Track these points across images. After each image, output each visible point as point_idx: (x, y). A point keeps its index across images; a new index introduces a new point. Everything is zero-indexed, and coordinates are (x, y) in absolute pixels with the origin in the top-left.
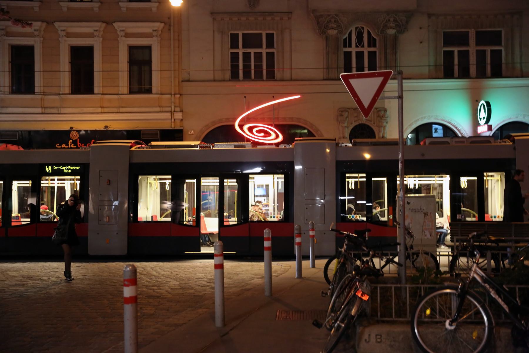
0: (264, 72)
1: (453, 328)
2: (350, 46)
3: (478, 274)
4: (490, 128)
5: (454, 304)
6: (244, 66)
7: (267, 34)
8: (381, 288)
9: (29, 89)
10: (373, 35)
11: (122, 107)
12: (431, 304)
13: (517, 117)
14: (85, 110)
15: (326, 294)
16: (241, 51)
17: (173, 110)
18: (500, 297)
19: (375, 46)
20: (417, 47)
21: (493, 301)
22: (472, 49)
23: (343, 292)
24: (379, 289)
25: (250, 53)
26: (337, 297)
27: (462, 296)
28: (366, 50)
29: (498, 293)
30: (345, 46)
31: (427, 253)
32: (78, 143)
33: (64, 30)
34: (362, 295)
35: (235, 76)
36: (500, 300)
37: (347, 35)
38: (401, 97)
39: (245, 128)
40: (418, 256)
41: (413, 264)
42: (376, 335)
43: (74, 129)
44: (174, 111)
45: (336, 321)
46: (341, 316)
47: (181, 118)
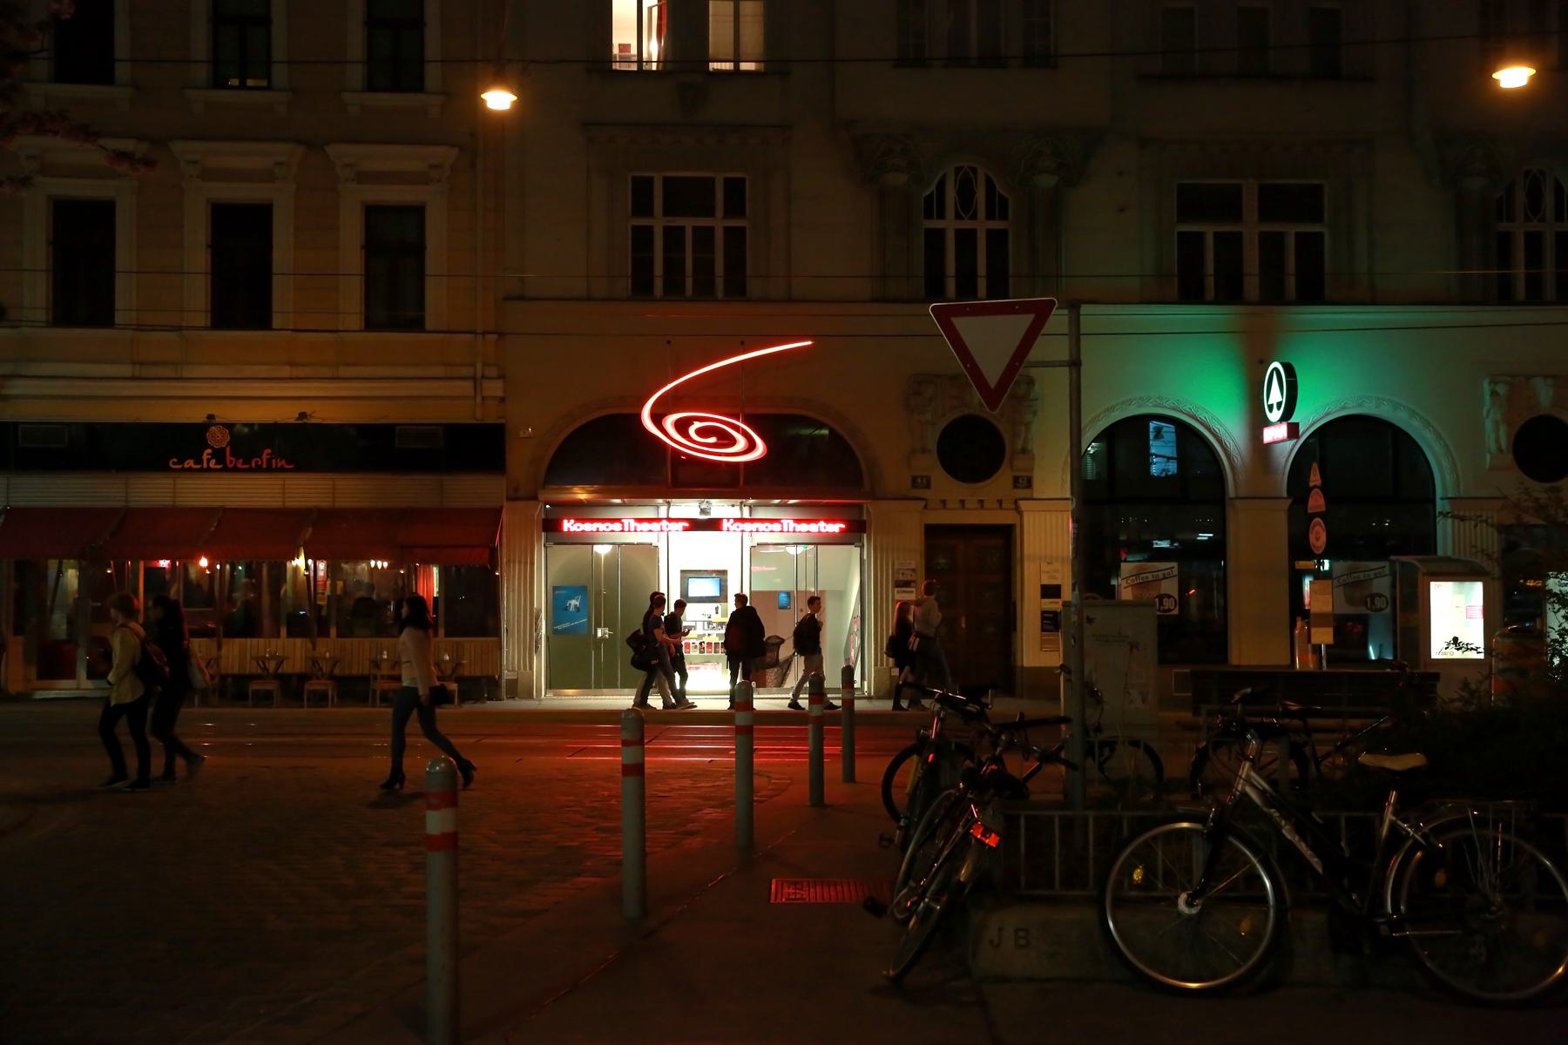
0: (720, 282)
1: (1194, 911)
2: (941, 215)
3: (1253, 786)
4: (1293, 431)
5: (1199, 855)
6: (666, 261)
7: (727, 181)
8: (1027, 817)
9: (100, 313)
10: (999, 189)
11: (348, 364)
12: (1144, 857)
13: (1360, 405)
14: (249, 371)
15: (891, 841)
16: (658, 223)
17: (479, 375)
18: (1303, 838)
19: (1004, 217)
20: (1111, 221)
21: (1288, 850)
22: (1251, 229)
23: (932, 836)
24: (1022, 822)
25: (682, 229)
26: (919, 846)
27: (1217, 837)
28: (982, 226)
29: (1299, 830)
30: (929, 215)
31: (1135, 743)
32: (228, 458)
33: (195, 162)
34: (983, 834)
35: (642, 286)
36: (1303, 847)
37: (933, 188)
38: (1075, 364)
39: (669, 421)
40: (1112, 750)
41: (1101, 769)
42: (1017, 930)
43: (218, 420)
44: (483, 377)
45: (922, 898)
46: (933, 888)
47: (500, 393)
